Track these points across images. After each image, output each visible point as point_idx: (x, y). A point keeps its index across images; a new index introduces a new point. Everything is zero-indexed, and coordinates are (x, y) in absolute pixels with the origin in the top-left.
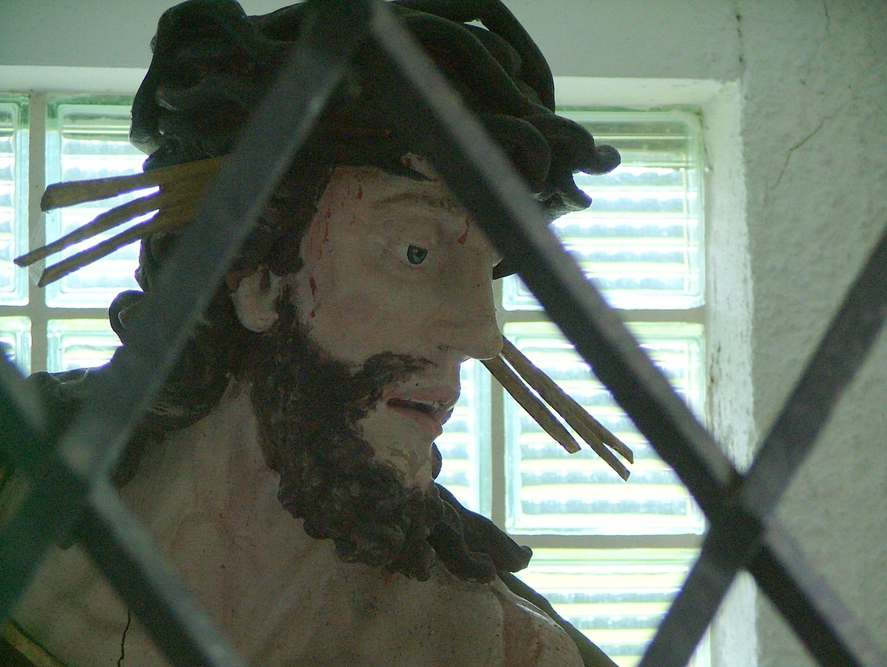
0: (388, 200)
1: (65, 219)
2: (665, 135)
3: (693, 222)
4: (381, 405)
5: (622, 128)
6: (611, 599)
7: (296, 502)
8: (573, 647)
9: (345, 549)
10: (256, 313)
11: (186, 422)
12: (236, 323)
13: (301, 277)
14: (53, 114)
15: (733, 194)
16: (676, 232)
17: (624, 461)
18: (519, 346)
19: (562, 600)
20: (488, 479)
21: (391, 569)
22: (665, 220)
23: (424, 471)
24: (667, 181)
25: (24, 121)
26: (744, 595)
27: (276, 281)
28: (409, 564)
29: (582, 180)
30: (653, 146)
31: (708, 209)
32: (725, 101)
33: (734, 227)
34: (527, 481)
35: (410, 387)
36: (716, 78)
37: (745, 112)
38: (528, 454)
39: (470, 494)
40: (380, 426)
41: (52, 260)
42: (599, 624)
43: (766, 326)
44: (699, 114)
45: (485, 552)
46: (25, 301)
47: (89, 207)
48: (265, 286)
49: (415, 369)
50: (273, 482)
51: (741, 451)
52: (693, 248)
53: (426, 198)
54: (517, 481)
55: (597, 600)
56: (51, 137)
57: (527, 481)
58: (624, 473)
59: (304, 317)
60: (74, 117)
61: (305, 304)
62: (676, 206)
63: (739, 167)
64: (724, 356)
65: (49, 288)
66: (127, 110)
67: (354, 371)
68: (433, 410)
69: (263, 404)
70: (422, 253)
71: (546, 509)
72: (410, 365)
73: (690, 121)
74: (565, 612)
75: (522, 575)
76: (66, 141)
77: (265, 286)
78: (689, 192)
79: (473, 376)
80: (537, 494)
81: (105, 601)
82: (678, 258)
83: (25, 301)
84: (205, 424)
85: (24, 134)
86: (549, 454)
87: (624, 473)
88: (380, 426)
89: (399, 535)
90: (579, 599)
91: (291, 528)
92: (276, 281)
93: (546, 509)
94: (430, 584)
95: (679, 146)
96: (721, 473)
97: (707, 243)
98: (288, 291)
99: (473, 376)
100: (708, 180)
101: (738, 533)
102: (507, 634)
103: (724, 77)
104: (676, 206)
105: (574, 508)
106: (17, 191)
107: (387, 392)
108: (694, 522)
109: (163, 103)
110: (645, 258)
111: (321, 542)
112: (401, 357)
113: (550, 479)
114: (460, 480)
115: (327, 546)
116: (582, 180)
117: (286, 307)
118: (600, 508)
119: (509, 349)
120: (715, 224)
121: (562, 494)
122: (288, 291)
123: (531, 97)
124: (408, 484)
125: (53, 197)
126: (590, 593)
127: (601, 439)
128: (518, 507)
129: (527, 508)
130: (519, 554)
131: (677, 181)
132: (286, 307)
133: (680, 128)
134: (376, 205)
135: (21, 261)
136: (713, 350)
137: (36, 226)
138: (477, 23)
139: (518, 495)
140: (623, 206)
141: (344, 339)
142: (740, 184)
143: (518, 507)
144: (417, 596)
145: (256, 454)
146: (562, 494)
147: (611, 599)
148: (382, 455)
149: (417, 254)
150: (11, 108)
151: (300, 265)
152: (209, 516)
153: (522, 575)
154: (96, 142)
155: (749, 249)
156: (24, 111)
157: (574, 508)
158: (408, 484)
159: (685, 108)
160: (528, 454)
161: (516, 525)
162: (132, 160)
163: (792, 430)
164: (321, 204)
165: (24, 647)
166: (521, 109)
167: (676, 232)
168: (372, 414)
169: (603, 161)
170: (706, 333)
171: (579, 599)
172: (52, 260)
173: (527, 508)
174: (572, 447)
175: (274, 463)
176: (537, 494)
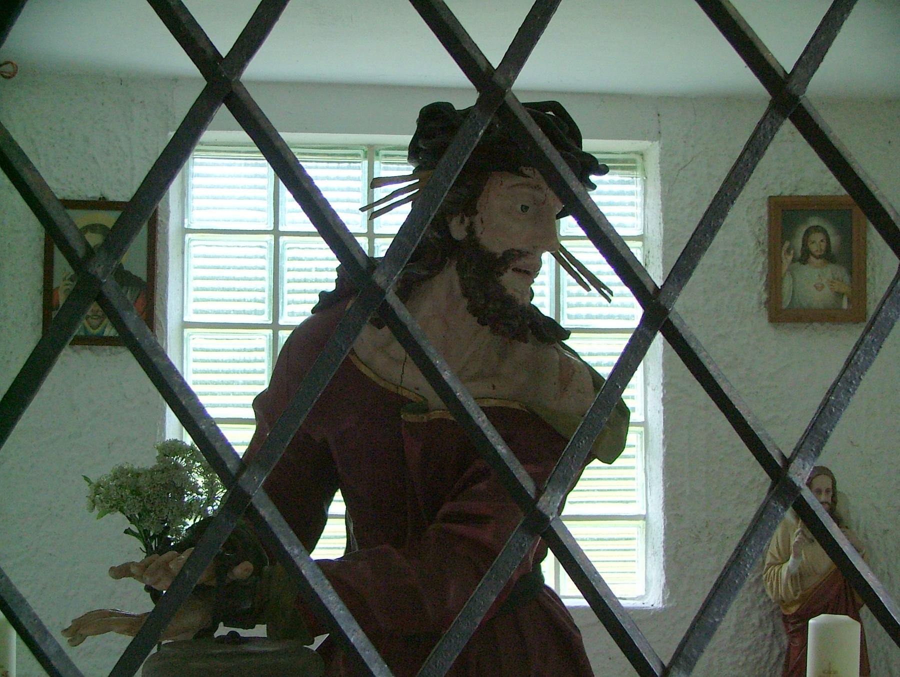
0: (514, 186)
1: (380, 193)
2: (628, 164)
3: (639, 200)
4: (510, 271)
5: (611, 161)
6: (603, 354)
7: (474, 310)
8: (586, 371)
9: (494, 330)
10: (458, 231)
11: (430, 277)
12: (450, 236)
13: (477, 218)
14: (377, 154)
15: (655, 188)
16: (632, 204)
17: (611, 297)
18: (568, 250)
19: (584, 355)
20: (554, 305)
21: (513, 338)
22: (627, 199)
23: (527, 298)
24: (628, 183)
25: (366, 157)
26: (659, 340)
27: (467, 220)
28: (519, 336)
29: (593, 178)
30: (623, 168)
31: (645, 195)
32: (652, 149)
33: (655, 202)
34: (570, 306)
35: (521, 263)
36: (649, 140)
37: (661, 154)
38: (570, 295)
39: (547, 311)
40: (508, 279)
41: (376, 208)
42: (598, 364)
43: (667, 242)
44: (642, 155)
45: (551, 332)
46: (365, 231)
47: (397, 213)
48: (462, 222)
49: (524, 256)
50: (465, 302)
51: (657, 275)
52: (639, 211)
53: (528, 185)
54: (566, 306)
55: (597, 355)
56: (377, 164)
57: (570, 306)
58: (610, 301)
59: (478, 234)
60: (386, 156)
61: (479, 228)
62: (632, 193)
63: (659, 177)
64: (651, 254)
65: (375, 220)
66: (406, 153)
67: (498, 256)
68: (531, 272)
69: (460, 269)
70: (527, 208)
71: (577, 317)
72: (521, 254)
73: (638, 158)
74: (584, 358)
75: (566, 342)
76: (383, 165)
77: (462, 222)
78: (638, 188)
79: (547, 258)
80: (573, 311)
81: (397, 349)
82: (633, 215)
83: (365, 231)
84: (437, 278)
85: (365, 163)
86: (579, 295)
87: (610, 301)
88: (508, 279)
89: (516, 324)
90: (590, 354)
91: (471, 320)
92: (467, 220)
93: (577, 317)
94: (529, 345)
95: (633, 169)
96: (650, 289)
97: (645, 197)
98: (471, 224)
99: (547, 258)
100: (645, 182)
101: (657, 315)
102: (560, 364)
103: (652, 139)
104: (632, 193)
105: (589, 317)
106: (364, 184)
107: (513, 265)
108: (638, 312)
109: (421, 146)
110: (618, 215)
111: (485, 327)
112: (518, 251)
113: (579, 305)
114: (542, 305)
115: (487, 328)
116: (593, 178)
117: (471, 230)
118: (598, 317)
119: (563, 249)
120: (648, 201)
121: (584, 311)
122: (471, 224)
123: (571, 143)
124: (520, 303)
125: (375, 183)
126: (595, 352)
127: (599, 286)
128: (566, 316)
129: (569, 317)
130: (566, 334)
131: (633, 183)
132: (471, 230)
133: (634, 161)
134: (509, 188)
135: (362, 209)
136: (646, 253)
137: (370, 195)
138: (550, 113)
139: (565, 311)
140: (610, 193)
141: (494, 242)
142: (658, 183)
143: (566, 316)
144: (523, 350)
145: (458, 290)
146: (584, 311)
147: (603, 354)
148: (510, 291)
149: (525, 208)
150: (360, 152)
151: (477, 213)
152: (439, 311)
153: (566, 342)
154: (395, 166)
155: (662, 211)
156: (366, 153)
157: (589, 317)
158: (520, 303)
159: (636, 153)
160: (570, 295)
161: (565, 323)
162: (408, 169)
163: (680, 271)
164: (486, 188)
165: (363, 369)
166: (569, 149)
167: (632, 204)
168: (505, 274)
169: (603, 170)
170: (643, 245)
171: (590, 354)
172: (376, 208)
173: (569, 317)
174: (588, 289)
175: (465, 295)
176: (573, 311)
